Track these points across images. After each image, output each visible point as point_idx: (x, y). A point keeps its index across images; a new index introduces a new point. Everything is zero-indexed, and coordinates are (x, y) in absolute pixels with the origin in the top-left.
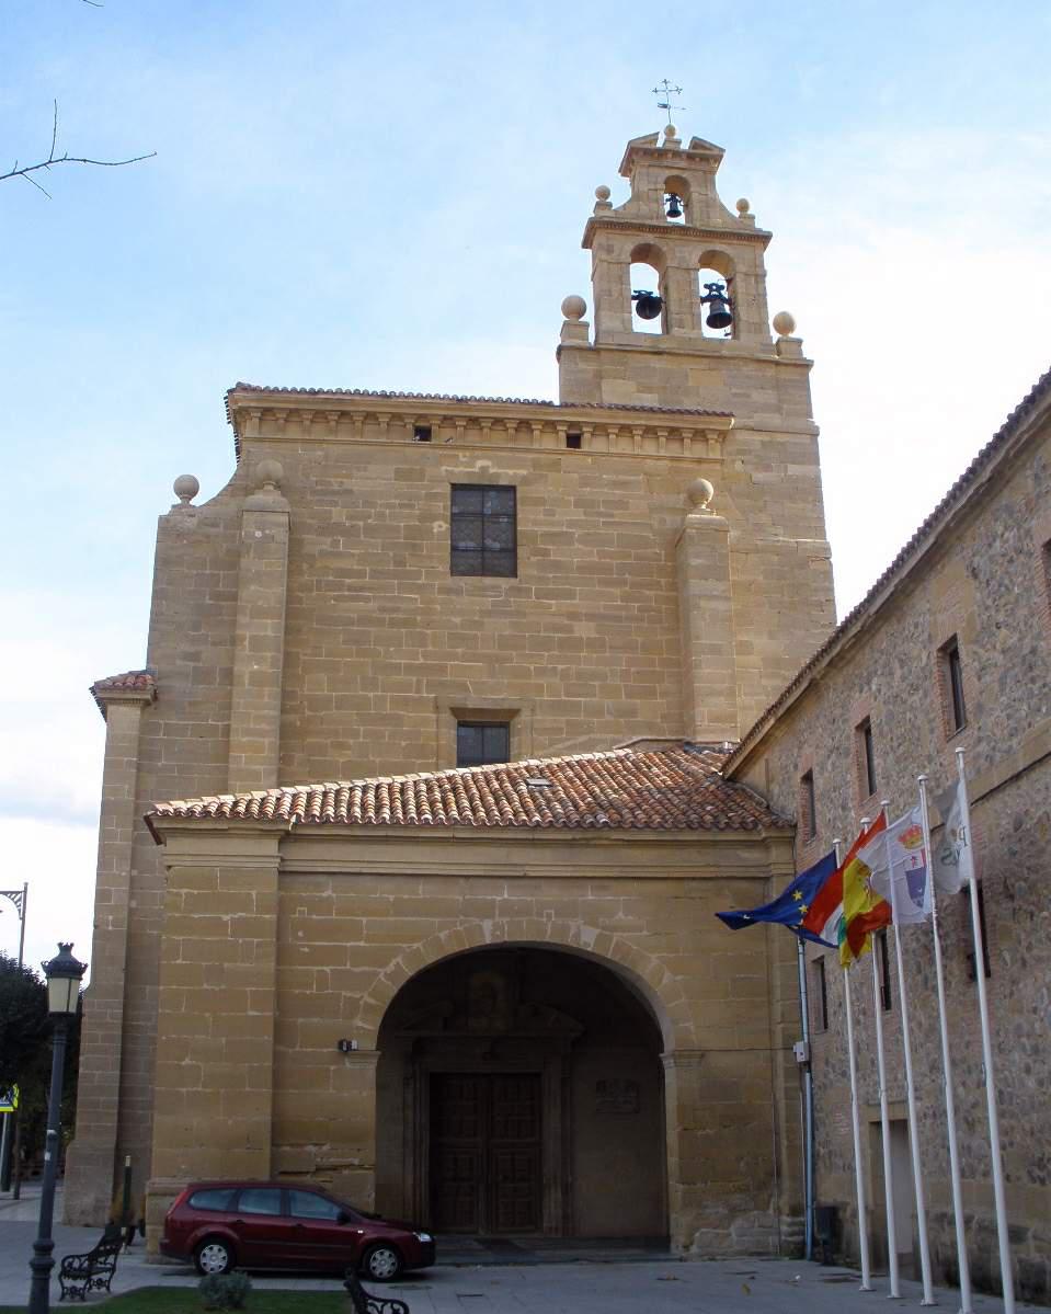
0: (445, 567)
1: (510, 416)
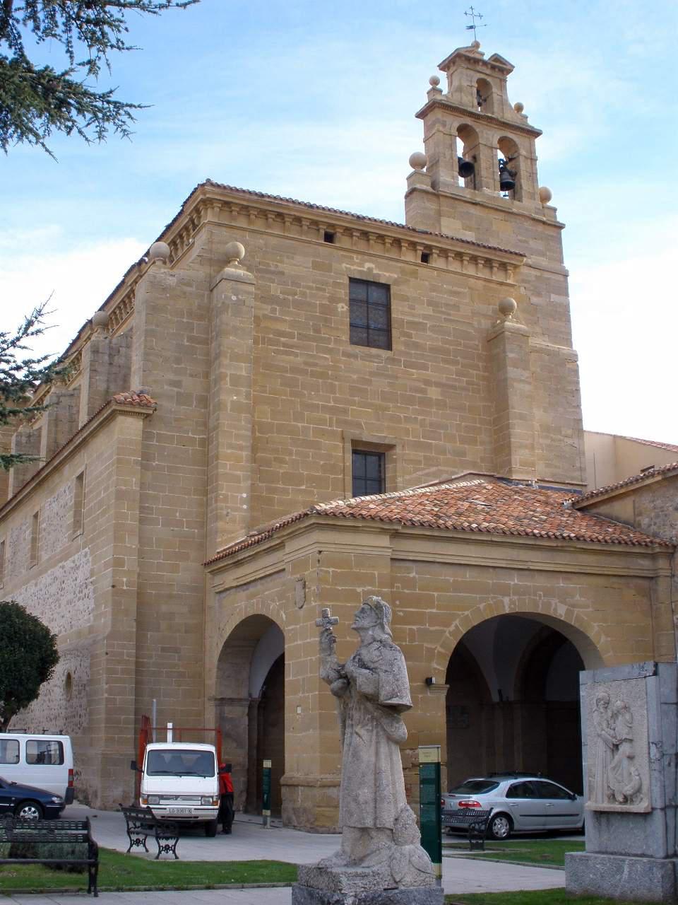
0: (345, 337)
1: (389, 234)
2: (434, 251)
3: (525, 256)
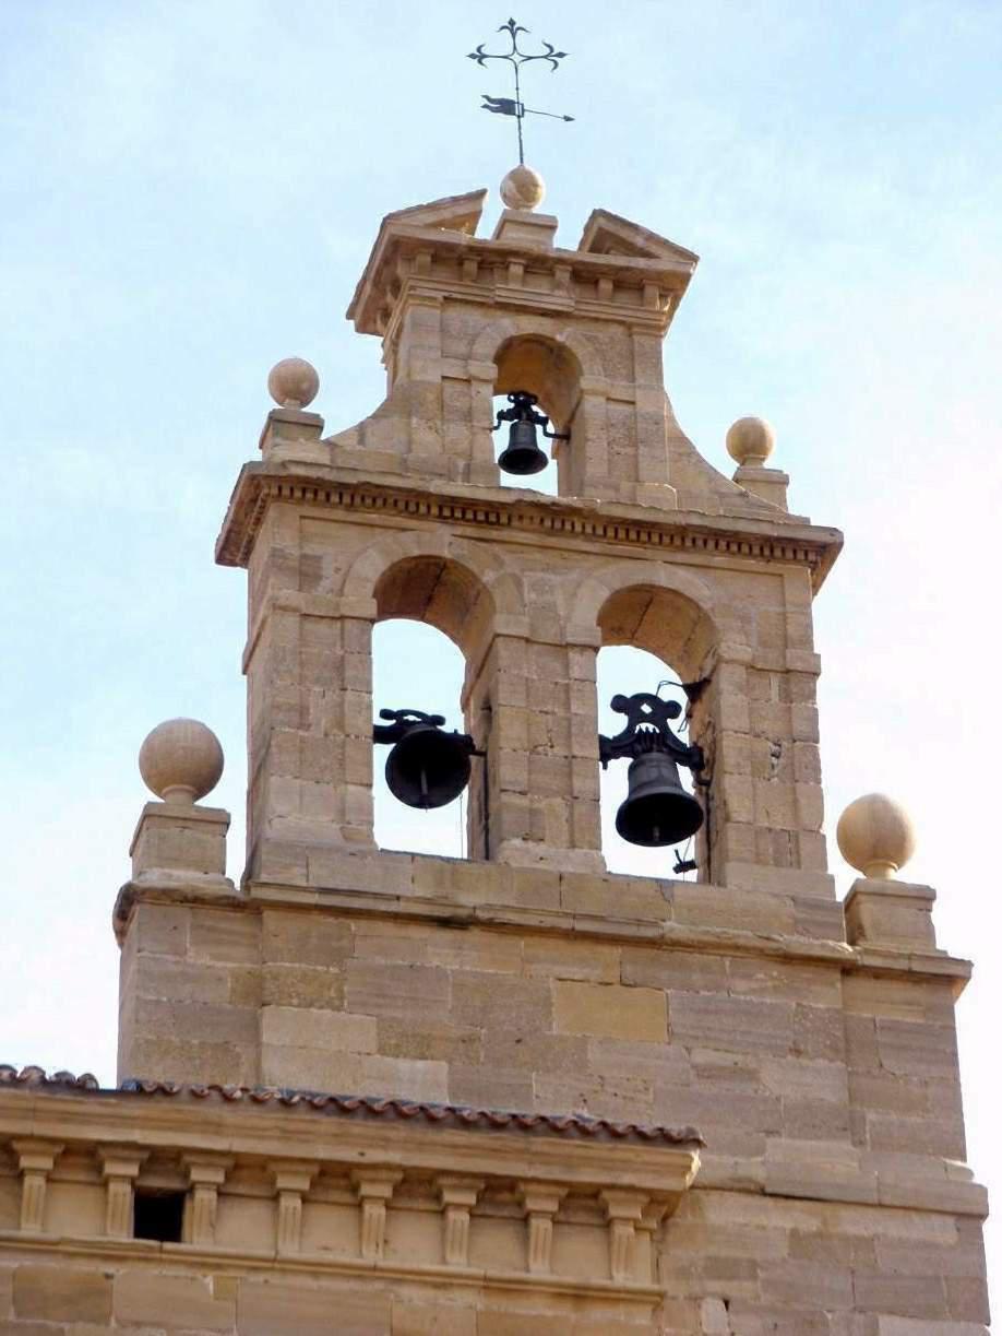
1: (627, 1179)
2: (195, 1175)
3: (698, 1143)
